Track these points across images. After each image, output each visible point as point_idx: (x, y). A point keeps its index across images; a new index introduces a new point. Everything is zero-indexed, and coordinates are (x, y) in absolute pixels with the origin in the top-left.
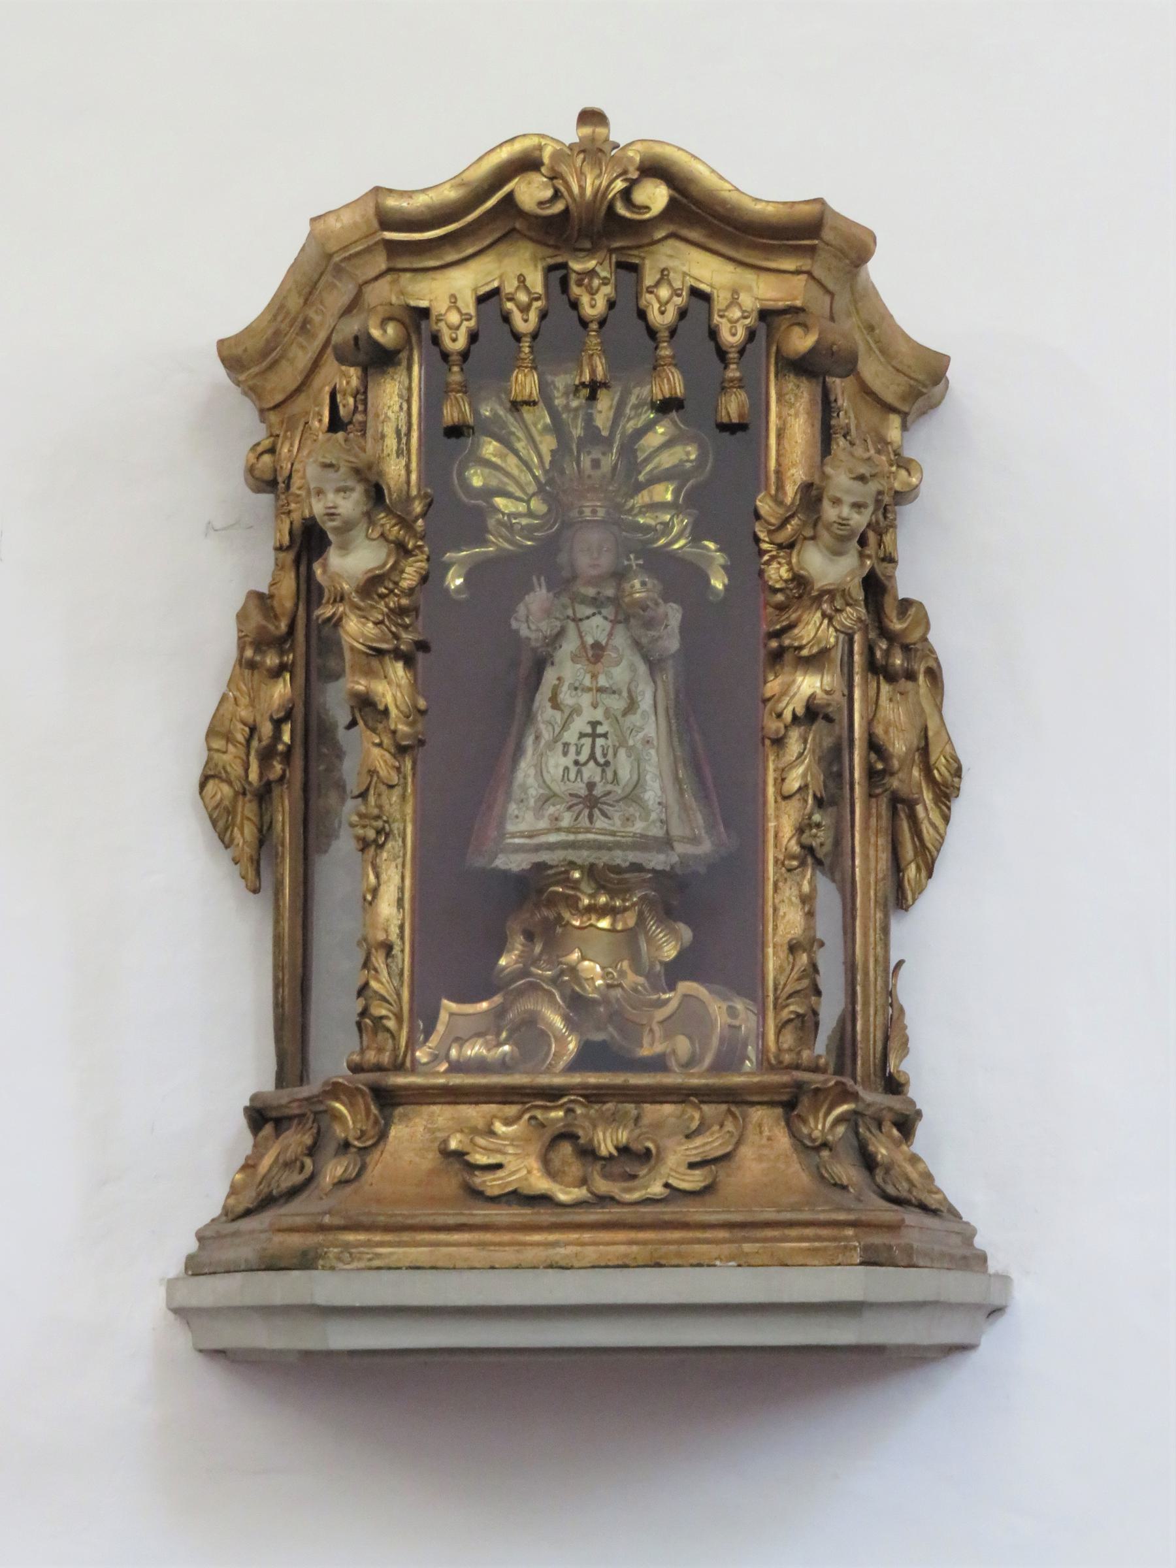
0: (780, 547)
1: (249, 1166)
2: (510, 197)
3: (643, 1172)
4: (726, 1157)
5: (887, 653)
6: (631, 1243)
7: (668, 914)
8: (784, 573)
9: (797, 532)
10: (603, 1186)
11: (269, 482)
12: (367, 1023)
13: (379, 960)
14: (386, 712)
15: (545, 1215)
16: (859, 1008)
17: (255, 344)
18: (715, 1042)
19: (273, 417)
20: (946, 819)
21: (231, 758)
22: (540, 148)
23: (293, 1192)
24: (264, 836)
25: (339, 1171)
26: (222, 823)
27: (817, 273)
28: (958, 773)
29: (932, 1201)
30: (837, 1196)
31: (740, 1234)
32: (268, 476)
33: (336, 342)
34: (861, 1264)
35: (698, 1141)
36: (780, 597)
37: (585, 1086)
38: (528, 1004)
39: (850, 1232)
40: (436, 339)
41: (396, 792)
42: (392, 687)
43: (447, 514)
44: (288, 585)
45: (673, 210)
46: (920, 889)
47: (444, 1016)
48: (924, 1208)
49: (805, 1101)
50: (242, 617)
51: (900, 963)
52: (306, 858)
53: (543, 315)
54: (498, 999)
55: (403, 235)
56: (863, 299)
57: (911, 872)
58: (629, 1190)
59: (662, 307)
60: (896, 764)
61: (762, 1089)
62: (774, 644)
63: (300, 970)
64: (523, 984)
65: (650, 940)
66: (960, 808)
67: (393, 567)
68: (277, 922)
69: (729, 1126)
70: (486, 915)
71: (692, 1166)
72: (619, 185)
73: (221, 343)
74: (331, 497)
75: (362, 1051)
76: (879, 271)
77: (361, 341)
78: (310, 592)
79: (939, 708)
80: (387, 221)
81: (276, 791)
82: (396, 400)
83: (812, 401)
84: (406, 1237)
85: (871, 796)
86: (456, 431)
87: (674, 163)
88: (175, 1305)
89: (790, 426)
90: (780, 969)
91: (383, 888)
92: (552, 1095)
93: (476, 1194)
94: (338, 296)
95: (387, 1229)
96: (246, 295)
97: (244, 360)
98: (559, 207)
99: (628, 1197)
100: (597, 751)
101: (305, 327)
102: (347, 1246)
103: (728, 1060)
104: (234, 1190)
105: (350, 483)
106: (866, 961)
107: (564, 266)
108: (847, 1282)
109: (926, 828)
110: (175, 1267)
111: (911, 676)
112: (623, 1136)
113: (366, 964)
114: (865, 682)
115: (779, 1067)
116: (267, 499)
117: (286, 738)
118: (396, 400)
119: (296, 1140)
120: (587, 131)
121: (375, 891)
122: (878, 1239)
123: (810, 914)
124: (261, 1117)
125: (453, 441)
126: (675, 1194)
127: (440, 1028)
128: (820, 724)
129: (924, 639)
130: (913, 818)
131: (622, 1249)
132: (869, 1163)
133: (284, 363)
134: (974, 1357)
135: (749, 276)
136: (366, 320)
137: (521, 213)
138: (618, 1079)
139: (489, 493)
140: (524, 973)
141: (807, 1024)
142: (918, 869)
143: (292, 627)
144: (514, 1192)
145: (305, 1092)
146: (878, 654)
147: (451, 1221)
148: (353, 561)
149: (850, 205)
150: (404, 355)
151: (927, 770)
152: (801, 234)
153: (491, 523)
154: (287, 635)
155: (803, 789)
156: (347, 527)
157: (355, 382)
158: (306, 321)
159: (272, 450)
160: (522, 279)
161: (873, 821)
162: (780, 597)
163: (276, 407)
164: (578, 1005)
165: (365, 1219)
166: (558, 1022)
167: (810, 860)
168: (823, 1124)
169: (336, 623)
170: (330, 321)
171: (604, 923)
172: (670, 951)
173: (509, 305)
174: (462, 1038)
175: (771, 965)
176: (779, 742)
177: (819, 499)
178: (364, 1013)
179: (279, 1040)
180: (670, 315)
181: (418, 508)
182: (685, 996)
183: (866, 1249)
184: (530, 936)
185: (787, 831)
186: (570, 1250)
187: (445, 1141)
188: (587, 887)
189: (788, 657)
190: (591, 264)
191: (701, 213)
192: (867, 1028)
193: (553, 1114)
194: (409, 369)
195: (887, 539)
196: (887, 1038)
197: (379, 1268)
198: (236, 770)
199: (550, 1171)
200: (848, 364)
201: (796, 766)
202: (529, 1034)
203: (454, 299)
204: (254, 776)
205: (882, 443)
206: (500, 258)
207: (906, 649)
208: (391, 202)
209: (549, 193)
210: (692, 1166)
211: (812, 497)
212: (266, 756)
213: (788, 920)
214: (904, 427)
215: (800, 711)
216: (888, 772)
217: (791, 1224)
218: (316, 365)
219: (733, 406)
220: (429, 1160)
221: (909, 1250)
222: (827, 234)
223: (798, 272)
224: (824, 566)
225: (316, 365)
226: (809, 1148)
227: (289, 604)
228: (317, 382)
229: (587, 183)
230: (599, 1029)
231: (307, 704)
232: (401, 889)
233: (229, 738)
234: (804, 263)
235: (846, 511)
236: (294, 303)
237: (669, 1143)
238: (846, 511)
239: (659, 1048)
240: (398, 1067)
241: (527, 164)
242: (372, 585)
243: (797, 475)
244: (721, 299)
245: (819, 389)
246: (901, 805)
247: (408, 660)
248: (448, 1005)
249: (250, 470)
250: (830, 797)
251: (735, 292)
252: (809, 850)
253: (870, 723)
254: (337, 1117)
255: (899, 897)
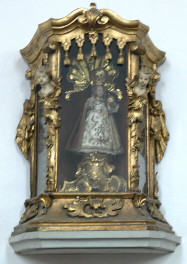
0: (131, 88)
1: (25, 214)
2: (77, 20)
3: (104, 211)
4: (120, 209)
5: (154, 111)
6: (100, 225)
7: (111, 163)
8: (131, 93)
9: (134, 84)
10: (95, 215)
11: (30, 78)
12: (48, 183)
13: (51, 169)
14: (52, 121)
15: (83, 220)
16: (148, 182)
17: (27, 50)
18: (119, 187)
19: (31, 65)
20: (166, 145)
21: (22, 132)
22: (83, 11)
23: (34, 217)
24: (29, 149)
25: (42, 212)
26: (20, 145)
27: (138, 35)
28: (168, 135)
29: (163, 220)
30: (143, 217)
31: (123, 224)
32: (29, 77)
33: (43, 47)
34: (147, 230)
35: (114, 206)
36: (131, 98)
37: (91, 195)
38: (82, 181)
39: (145, 223)
40: (63, 48)
41: (54, 137)
42: (54, 116)
43: (66, 84)
44: (34, 97)
45: (109, 23)
46: (161, 159)
47: (65, 185)
48: (160, 221)
49: (136, 198)
50: (24, 104)
51: (157, 173)
52: (37, 153)
53: (84, 43)
54: (75, 181)
55: (54, 27)
56: (148, 40)
57: (159, 156)
58: (101, 215)
59: (107, 41)
60: (155, 133)
61: (127, 195)
62: (130, 107)
63: (35, 174)
64: (81, 177)
65: (106, 168)
66: (169, 142)
67: (54, 92)
68: (31, 165)
69: (121, 203)
70: (72, 161)
71: (113, 211)
72: (98, 18)
73: (21, 50)
74: (41, 78)
75: (47, 188)
76: (150, 34)
77: (48, 48)
78: (38, 98)
79: (165, 122)
80: (53, 25)
81: (31, 139)
82: (55, 59)
83: (137, 60)
84: (56, 224)
85: (151, 140)
86: (67, 66)
87: (109, 13)
88: (11, 242)
89: (132, 63)
90: (131, 172)
91: (52, 156)
92: (85, 197)
93: (70, 216)
94: (43, 40)
95: (52, 223)
96: (25, 41)
97: (25, 53)
98: (87, 22)
99: (100, 217)
100: (95, 131)
101: (37, 47)
102: (44, 226)
103: (121, 190)
104: (22, 218)
105: (46, 75)
106: (150, 172)
107: (88, 34)
108: (146, 233)
109: (162, 147)
110: (9, 235)
111: (159, 116)
112: (99, 205)
113: (48, 171)
114: (149, 117)
115: (131, 191)
116: (29, 81)
117: (33, 128)
118: (55, 59)
119: (34, 208)
120: (92, 7)
121: (50, 156)
122: (150, 225)
123: (137, 161)
124: (27, 204)
125: (66, 68)
126: (109, 216)
127: (64, 187)
128: (138, 123)
129: (161, 108)
130: (159, 144)
131: (99, 227)
132: (149, 211)
133: (33, 54)
134: (173, 254)
135: (125, 35)
136: (49, 44)
137: (79, 23)
138: (98, 194)
139: (74, 80)
140: (81, 175)
141: (137, 182)
142: (161, 155)
143: (34, 107)
144: (77, 216)
145: (36, 198)
146: (152, 111)
147: (65, 221)
148: (46, 91)
149: (144, 21)
150: (56, 51)
151: (162, 135)
152: (134, 27)
153: (74, 86)
154: (33, 108)
155: (135, 136)
156: (45, 84)
157: (47, 57)
158: (37, 45)
159: (30, 71)
160: (80, 36)
161: (151, 145)
162: (131, 98)
163: (32, 63)
164: (92, 181)
165: (47, 221)
166: (87, 184)
167: (137, 150)
168: (140, 202)
169: (42, 103)
170: (42, 45)
171: (97, 164)
172: (111, 170)
173: (77, 41)
174: (68, 188)
175: (129, 171)
176: (131, 126)
177: (138, 78)
178: (48, 181)
179: (31, 189)
180: (109, 43)
181: (59, 80)
182: (113, 179)
183: (148, 227)
184: (82, 168)
185: (132, 144)
186: (89, 227)
187: (64, 206)
188: (94, 157)
189: (133, 110)
190: (93, 33)
191: (114, 23)
192: (150, 185)
193: (85, 200)
194: (57, 54)
195: (153, 88)
196: (154, 188)
197: (50, 231)
198: (23, 135)
199: (85, 211)
200: (144, 52)
201: (133, 131)
202: (82, 187)
203: (66, 40)
204: (26, 136)
205: (152, 69)
206: (76, 32)
207: (158, 110)
208: (54, 21)
209: (85, 19)
210: (113, 211)
211: (137, 78)
212: (29, 132)
213: (132, 161)
214: (157, 67)
215: (135, 120)
216: (154, 135)
217: (133, 222)
218: (39, 54)
219: (121, 60)
220: (60, 210)
221: (157, 228)
222: (140, 27)
223: (134, 34)
224: (140, 91)
225: (39, 54)
226: (136, 207)
227: (34, 102)
228: (40, 58)
229: (92, 18)
230: (96, 186)
231: (37, 121)
232: (55, 156)
233: (22, 129)
234: (136, 33)
235: (143, 80)
236: (35, 42)
237: (109, 206)
238: (143, 80)
239: (108, 189)
240: (54, 191)
241: (80, 14)
242: (49, 95)
243: (134, 74)
244: (119, 40)
245: (138, 58)
246: (157, 142)
247: (57, 110)
248: (66, 182)
249: (26, 75)
250: (141, 139)
251: (122, 38)
252: (136, 148)
253: (150, 125)
254: (42, 201)
255: (157, 161)
